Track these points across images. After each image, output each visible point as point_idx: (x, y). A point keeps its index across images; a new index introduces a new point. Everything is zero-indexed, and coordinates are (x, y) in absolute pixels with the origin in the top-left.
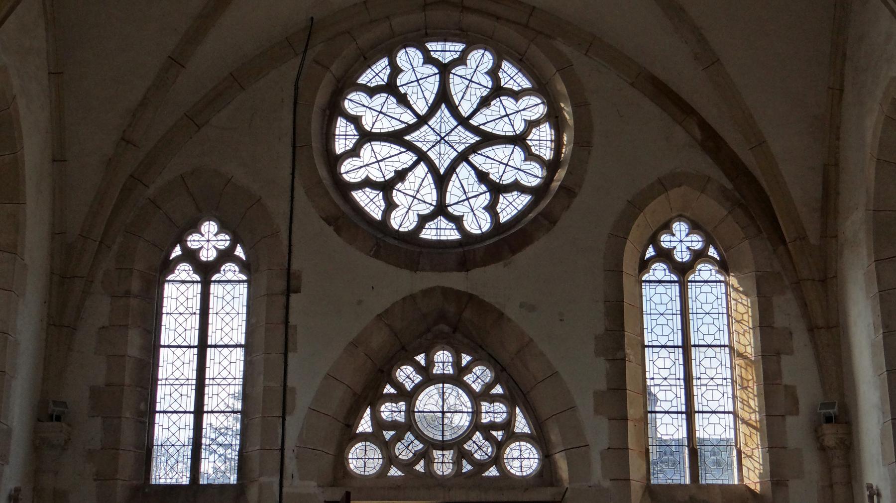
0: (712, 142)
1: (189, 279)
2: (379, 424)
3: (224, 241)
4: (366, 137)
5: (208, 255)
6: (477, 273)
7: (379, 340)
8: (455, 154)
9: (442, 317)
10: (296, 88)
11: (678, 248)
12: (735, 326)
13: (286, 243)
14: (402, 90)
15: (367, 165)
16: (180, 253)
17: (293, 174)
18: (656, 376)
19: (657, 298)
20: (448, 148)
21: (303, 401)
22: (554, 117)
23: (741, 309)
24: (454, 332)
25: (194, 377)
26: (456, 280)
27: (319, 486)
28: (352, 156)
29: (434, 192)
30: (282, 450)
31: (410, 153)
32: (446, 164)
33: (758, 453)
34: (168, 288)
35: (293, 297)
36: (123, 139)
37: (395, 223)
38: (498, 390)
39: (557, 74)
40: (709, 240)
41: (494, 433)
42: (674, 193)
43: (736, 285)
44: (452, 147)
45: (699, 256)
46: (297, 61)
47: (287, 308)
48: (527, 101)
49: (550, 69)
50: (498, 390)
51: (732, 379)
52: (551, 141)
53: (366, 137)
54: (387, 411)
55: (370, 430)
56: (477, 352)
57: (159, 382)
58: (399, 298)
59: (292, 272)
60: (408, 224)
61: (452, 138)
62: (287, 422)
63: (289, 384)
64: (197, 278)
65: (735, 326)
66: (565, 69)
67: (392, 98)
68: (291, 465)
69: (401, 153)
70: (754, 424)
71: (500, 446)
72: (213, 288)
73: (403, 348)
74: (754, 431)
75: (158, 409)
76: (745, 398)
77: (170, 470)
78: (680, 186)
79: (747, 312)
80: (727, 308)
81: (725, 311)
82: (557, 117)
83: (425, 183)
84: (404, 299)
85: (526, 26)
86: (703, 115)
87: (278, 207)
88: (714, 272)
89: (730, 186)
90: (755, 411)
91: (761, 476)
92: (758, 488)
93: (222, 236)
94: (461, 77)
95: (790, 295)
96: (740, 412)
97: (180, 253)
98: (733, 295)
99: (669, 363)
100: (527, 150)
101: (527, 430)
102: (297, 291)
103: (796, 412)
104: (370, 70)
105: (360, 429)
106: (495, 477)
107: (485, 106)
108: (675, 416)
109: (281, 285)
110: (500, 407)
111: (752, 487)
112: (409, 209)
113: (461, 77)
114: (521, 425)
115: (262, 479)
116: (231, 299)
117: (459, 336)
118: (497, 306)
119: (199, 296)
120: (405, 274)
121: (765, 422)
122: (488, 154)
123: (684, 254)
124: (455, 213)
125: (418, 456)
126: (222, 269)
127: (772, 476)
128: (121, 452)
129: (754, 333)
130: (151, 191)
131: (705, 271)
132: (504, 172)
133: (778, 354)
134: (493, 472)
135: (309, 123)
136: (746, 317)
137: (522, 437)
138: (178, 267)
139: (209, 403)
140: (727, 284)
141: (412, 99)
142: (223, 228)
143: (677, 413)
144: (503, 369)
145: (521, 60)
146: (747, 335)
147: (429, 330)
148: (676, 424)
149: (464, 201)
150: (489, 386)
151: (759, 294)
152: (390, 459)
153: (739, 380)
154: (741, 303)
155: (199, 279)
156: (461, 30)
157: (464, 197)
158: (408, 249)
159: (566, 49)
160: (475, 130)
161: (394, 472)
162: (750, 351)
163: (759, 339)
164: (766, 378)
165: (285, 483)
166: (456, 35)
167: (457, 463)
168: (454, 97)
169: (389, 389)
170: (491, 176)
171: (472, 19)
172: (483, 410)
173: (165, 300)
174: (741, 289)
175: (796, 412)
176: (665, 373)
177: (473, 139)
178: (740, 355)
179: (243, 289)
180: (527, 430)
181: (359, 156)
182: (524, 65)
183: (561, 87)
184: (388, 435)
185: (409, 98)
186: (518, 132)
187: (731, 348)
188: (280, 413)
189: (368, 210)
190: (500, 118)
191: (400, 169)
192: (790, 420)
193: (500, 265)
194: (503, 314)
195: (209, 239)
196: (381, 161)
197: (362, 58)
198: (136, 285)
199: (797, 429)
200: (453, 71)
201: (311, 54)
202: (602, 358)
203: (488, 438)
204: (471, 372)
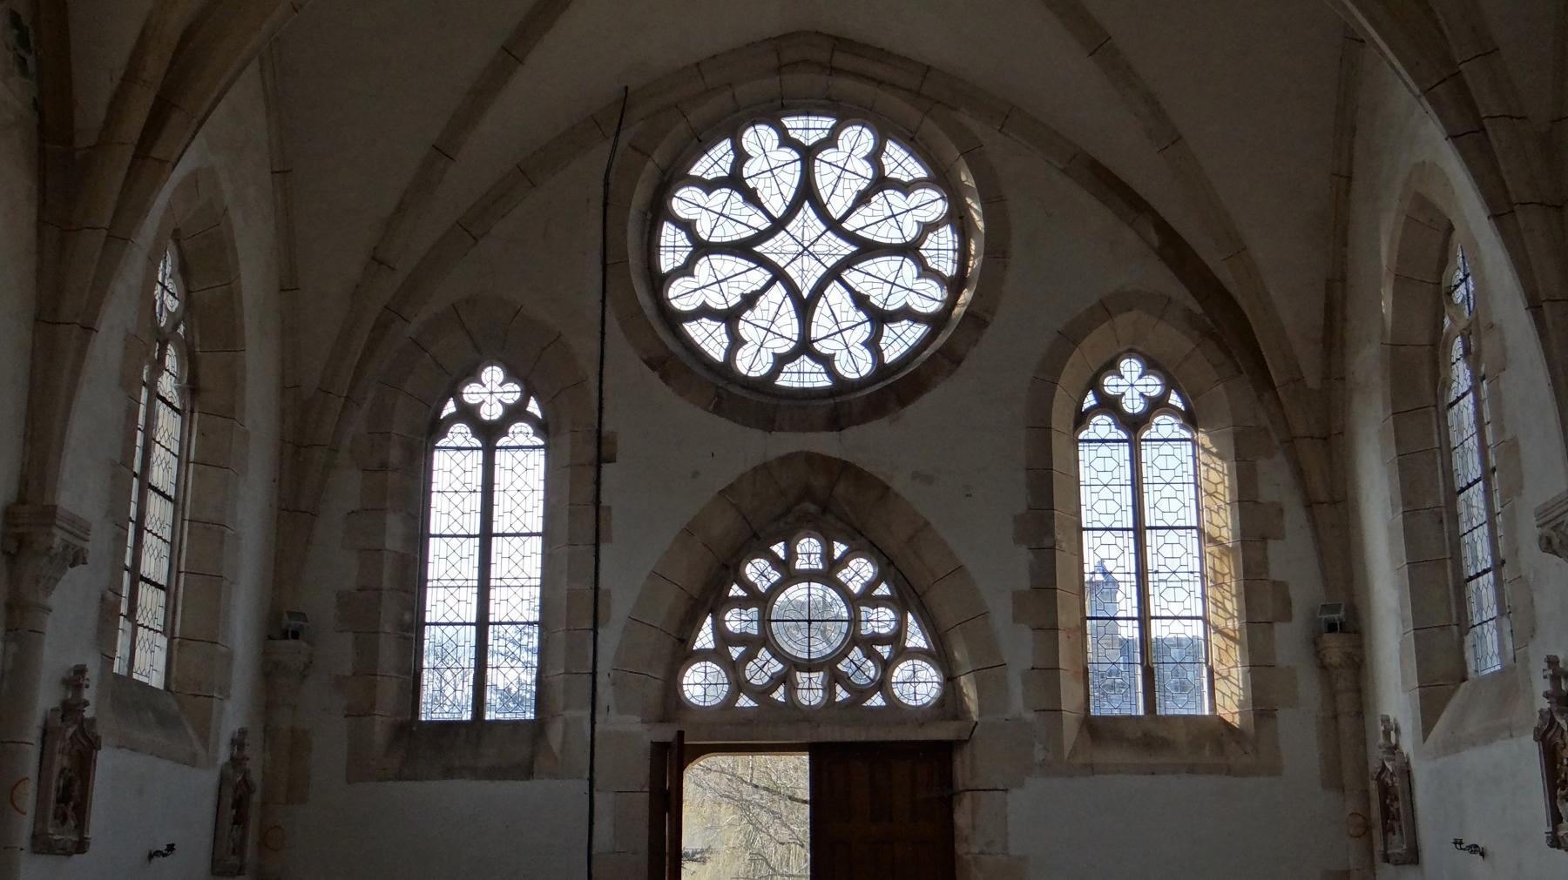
0: (1175, 251)
3: (513, 392)
5: (491, 412)
6: (852, 434)
9: (807, 493)
10: (606, 184)
11: (1128, 395)
13: (595, 394)
17: (603, 301)
20: (814, 262)
21: (620, 606)
22: (957, 218)
23: (1214, 477)
26: (825, 443)
27: (643, 722)
29: (795, 322)
30: (594, 674)
33: (1237, 674)
34: (438, 457)
35: (606, 468)
38: (883, 590)
39: (962, 160)
42: (1123, 319)
43: (1208, 444)
45: (1156, 405)
46: (608, 146)
47: (598, 483)
48: (920, 196)
49: (952, 152)
54: (735, 621)
60: (759, 367)
63: (603, 585)
64: (477, 443)
65: (1205, 501)
68: (605, 695)
71: (886, 666)
73: (755, 535)
76: (1219, 598)
80: (1195, 476)
85: (918, 94)
90: (1232, 616)
91: (1241, 705)
92: (1236, 721)
95: (1280, 458)
96: (1212, 617)
98: (1203, 457)
100: (920, 262)
101: (922, 644)
102: (612, 460)
103: (1287, 616)
105: (698, 645)
106: (880, 707)
109: (591, 451)
111: (1229, 719)
114: (916, 639)
115: (568, 714)
116: (524, 472)
120: (757, 434)
123: (1137, 403)
124: (824, 351)
127: (1254, 704)
131: (1165, 426)
133: (1264, 539)
134: (877, 700)
136: (1220, 488)
137: (916, 653)
139: (496, 613)
140: (1194, 443)
141: (763, 195)
146: (1222, 513)
147: (788, 511)
152: (739, 685)
153: (1210, 574)
156: (829, 98)
158: (759, 401)
161: (744, 701)
164: (1247, 570)
165: (598, 718)
166: (819, 107)
170: (872, 300)
171: (844, 85)
175: (1287, 616)
177: (848, 249)
178: (1212, 540)
179: (539, 458)
180: (922, 644)
182: (917, 147)
183: (966, 178)
184: (736, 652)
192: (1279, 628)
195: (492, 391)
198: (395, 455)
203: (871, 654)
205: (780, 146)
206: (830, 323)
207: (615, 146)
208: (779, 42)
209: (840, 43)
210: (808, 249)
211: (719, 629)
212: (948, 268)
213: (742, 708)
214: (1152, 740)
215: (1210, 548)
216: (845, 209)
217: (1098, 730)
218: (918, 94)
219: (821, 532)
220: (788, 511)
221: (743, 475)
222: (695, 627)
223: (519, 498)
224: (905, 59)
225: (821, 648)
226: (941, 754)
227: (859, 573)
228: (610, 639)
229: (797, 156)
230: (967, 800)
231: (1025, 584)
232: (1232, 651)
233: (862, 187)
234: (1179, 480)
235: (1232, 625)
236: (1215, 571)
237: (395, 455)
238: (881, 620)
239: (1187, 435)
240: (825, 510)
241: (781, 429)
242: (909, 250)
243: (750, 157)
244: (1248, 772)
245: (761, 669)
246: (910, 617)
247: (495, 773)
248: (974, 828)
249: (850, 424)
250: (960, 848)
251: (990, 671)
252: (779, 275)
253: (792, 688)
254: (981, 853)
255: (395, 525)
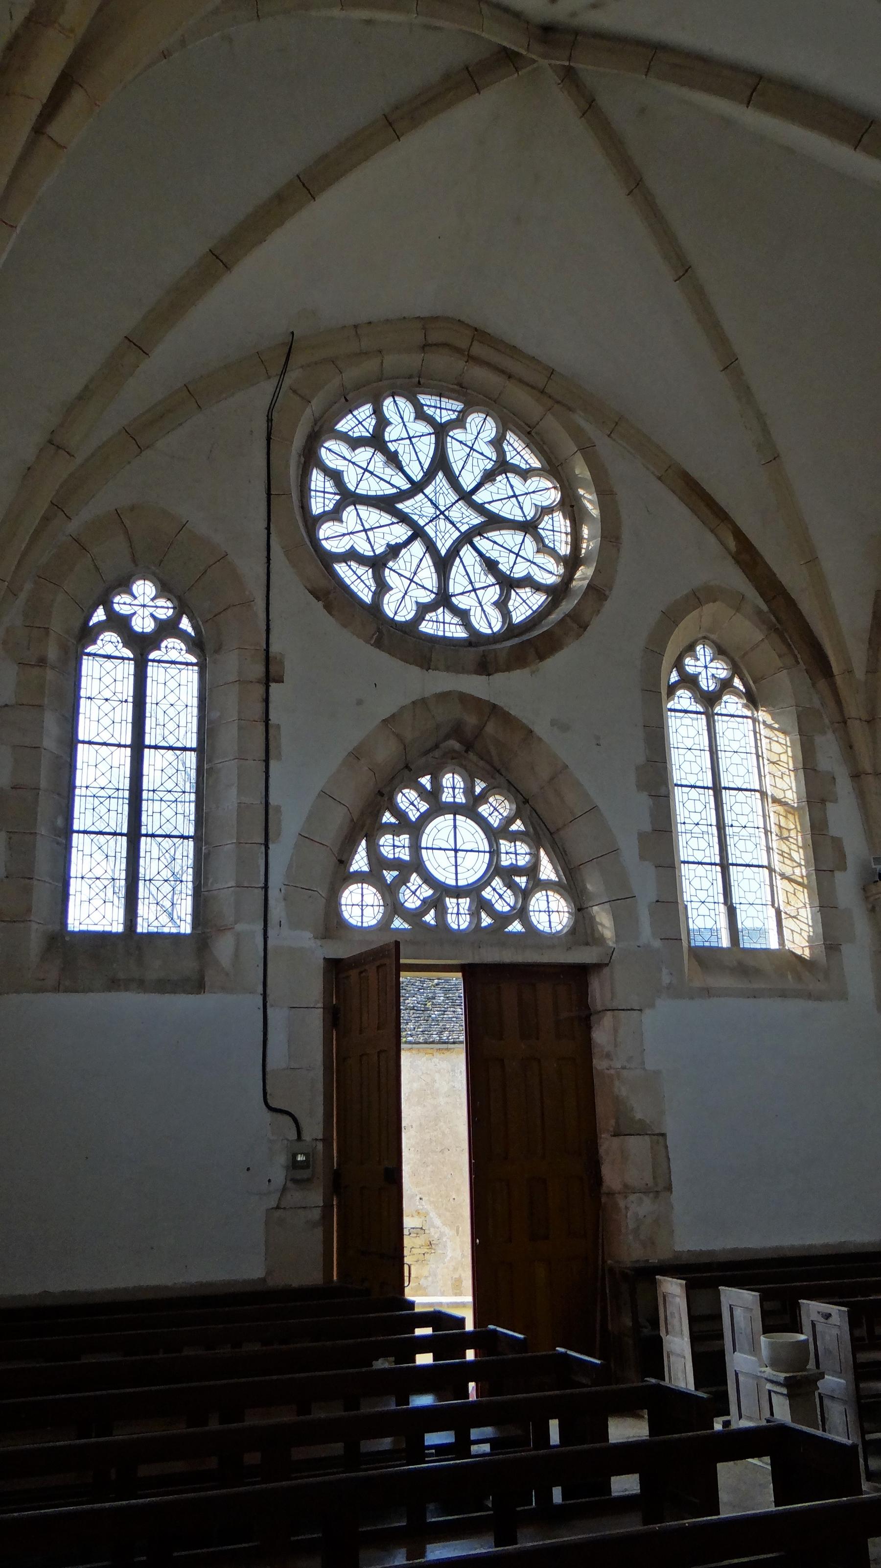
0: (747, 556)
1: (117, 654)
2: (377, 861)
3: (165, 610)
4: (349, 498)
5: (143, 624)
6: (499, 678)
7: (386, 752)
8: (457, 534)
9: (457, 731)
10: (270, 420)
11: (704, 675)
12: (768, 768)
13: (262, 615)
14: (392, 447)
15: (352, 533)
16: (104, 618)
17: (268, 528)
18: (687, 821)
19: (684, 730)
20: (449, 526)
21: (291, 823)
22: (570, 506)
23: (777, 748)
24: (466, 751)
25: (127, 786)
26: (475, 685)
27: (316, 938)
28: (333, 520)
29: (435, 576)
30: (266, 888)
31: (404, 525)
32: (448, 544)
33: (806, 914)
34: (87, 664)
35: (273, 686)
36: (51, 442)
37: (389, 609)
38: (518, 826)
39: (579, 454)
40: (736, 670)
41: (517, 879)
42: (709, 609)
43: (769, 721)
44: (454, 525)
45: (725, 685)
46: (268, 387)
47: (267, 701)
48: (535, 483)
49: (568, 447)
50: (518, 826)
51: (765, 828)
52: (567, 534)
53: (349, 498)
54: (395, 846)
55: (366, 869)
56: (493, 777)
57: (77, 792)
58: (408, 701)
59: (271, 655)
60: (404, 612)
61: (454, 514)
62: (270, 852)
63: (272, 801)
64: (128, 653)
65: (768, 768)
66: (588, 451)
67: (379, 454)
68: (277, 910)
69: (393, 523)
70: (800, 880)
71: (525, 895)
72: (152, 670)
73: (407, 767)
74: (801, 889)
75: (76, 828)
76: (786, 850)
77: (92, 908)
78: (714, 601)
79: (786, 752)
80: (756, 747)
81: (754, 751)
82: (572, 506)
83: (424, 564)
84: (413, 702)
85: (542, 392)
86: (739, 523)
87: (251, 569)
88: (740, 706)
89: (764, 607)
90: (800, 865)
91: (810, 939)
92: (807, 954)
93: (161, 602)
94: (461, 442)
95: (830, 736)
96: (777, 866)
97: (104, 618)
98: (764, 731)
99: (699, 807)
100: (539, 539)
101: (553, 877)
102: (280, 680)
103: (844, 868)
104: (350, 416)
105: (354, 867)
106: (519, 933)
107: (491, 481)
108: (708, 867)
109: (258, 670)
110: (522, 848)
111: (799, 952)
112: (406, 593)
113: (461, 442)
114: (547, 871)
115: (239, 927)
116: (176, 686)
117: (472, 756)
118: (524, 721)
119: (132, 678)
120: (415, 671)
121: (814, 877)
122: (495, 539)
123: (710, 682)
124: (461, 606)
125: (427, 904)
126: (163, 644)
127: (825, 939)
128: (35, 882)
129: (796, 776)
130: (73, 527)
131: (731, 704)
132: (515, 563)
133: (823, 801)
134: (516, 927)
135: (287, 466)
136: (784, 758)
137: (547, 885)
138: (101, 637)
139: (149, 822)
140: (755, 720)
141: (404, 459)
142: (164, 589)
143: (711, 864)
144: (526, 801)
145: (529, 433)
146: (786, 778)
147: (437, 746)
148: (710, 878)
149: (470, 591)
150: (510, 821)
151: (801, 732)
152: (394, 907)
153: (774, 829)
154: (777, 742)
155: (131, 656)
156: (460, 385)
157: (470, 588)
158: (404, 641)
159: (589, 428)
160: (480, 509)
161: (398, 923)
162: (791, 796)
163: (803, 782)
164: (813, 827)
165: (270, 933)
166: (453, 391)
167: (475, 914)
168: (454, 465)
169: (388, 818)
170: (500, 566)
171: (479, 374)
172: (503, 850)
173: (83, 680)
174: (776, 726)
175: (844, 868)
176: (696, 818)
177: (476, 520)
178: (775, 801)
179: (191, 676)
180: (553, 877)
181: (340, 520)
182: (534, 439)
183: (581, 470)
184: (389, 876)
185: (400, 458)
186: (529, 518)
187: (763, 794)
188: (262, 840)
189: (356, 590)
190: (374, 531)
191: (393, 543)
192: (838, 875)
193: (527, 671)
194: (531, 732)
195: (143, 603)
196: (369, 530)
197: (343, 400)
198: (53, 653)
199: (846, 885)
200: (451, 434)
201: (288, 381)
202: (646, 793)
203: (511, 885)
204: (487, 802)
205: (416, 418)
206: (466, 582)
207: (279, 386)
208: (426, 322)
209: (479, 334)
210: (440, 517)
211: (373, 853)
212: (564, 549)
213: (397, 929)
214: (739, 967)
215: (772, 808)
216: (474, 484)
217: (706, 957)
218: (542, 392)
219: (465, 768)
220: (437, 746)
221: (403, 708)
222: (353, 851)
223: (172, 712)
224: (533, 359)
225: (467, 878)
226: (580, 974)
227: (495, 810)
228: (281, 854)
229: (432, 431)
230: (607, 1020)
231: (647, 827)
232: (800, 895)
233: (489, 467)
234: (743, 750)
235: (799, 872)
236: (780, 827)
237: (53, 653)
238: (515, 853)
239: (749, 714)
240: (469, 746)
241: (436, 669)
242: (529, 527)
243: (390, 423)
244: (819, 998)
245: (415, 893)
246: (542, 853)
247: (164, 986)
248: (616, 1046)
249: (497, 670)
250: (599, 1064)
251: (622, 903)
252: (418, 533)
253: (442, 912)
254: (624, 1068)
255: (51, 724)
